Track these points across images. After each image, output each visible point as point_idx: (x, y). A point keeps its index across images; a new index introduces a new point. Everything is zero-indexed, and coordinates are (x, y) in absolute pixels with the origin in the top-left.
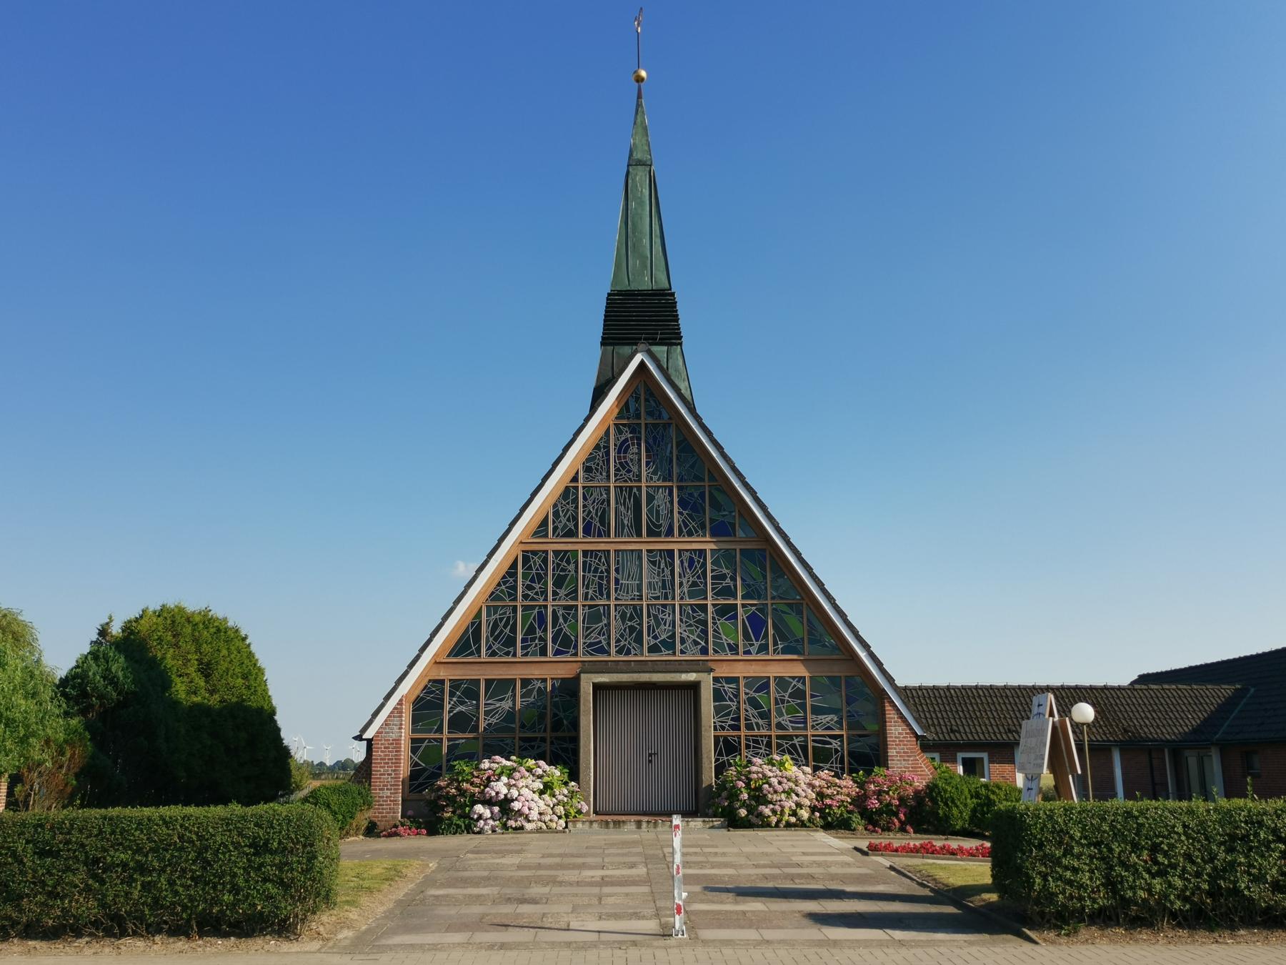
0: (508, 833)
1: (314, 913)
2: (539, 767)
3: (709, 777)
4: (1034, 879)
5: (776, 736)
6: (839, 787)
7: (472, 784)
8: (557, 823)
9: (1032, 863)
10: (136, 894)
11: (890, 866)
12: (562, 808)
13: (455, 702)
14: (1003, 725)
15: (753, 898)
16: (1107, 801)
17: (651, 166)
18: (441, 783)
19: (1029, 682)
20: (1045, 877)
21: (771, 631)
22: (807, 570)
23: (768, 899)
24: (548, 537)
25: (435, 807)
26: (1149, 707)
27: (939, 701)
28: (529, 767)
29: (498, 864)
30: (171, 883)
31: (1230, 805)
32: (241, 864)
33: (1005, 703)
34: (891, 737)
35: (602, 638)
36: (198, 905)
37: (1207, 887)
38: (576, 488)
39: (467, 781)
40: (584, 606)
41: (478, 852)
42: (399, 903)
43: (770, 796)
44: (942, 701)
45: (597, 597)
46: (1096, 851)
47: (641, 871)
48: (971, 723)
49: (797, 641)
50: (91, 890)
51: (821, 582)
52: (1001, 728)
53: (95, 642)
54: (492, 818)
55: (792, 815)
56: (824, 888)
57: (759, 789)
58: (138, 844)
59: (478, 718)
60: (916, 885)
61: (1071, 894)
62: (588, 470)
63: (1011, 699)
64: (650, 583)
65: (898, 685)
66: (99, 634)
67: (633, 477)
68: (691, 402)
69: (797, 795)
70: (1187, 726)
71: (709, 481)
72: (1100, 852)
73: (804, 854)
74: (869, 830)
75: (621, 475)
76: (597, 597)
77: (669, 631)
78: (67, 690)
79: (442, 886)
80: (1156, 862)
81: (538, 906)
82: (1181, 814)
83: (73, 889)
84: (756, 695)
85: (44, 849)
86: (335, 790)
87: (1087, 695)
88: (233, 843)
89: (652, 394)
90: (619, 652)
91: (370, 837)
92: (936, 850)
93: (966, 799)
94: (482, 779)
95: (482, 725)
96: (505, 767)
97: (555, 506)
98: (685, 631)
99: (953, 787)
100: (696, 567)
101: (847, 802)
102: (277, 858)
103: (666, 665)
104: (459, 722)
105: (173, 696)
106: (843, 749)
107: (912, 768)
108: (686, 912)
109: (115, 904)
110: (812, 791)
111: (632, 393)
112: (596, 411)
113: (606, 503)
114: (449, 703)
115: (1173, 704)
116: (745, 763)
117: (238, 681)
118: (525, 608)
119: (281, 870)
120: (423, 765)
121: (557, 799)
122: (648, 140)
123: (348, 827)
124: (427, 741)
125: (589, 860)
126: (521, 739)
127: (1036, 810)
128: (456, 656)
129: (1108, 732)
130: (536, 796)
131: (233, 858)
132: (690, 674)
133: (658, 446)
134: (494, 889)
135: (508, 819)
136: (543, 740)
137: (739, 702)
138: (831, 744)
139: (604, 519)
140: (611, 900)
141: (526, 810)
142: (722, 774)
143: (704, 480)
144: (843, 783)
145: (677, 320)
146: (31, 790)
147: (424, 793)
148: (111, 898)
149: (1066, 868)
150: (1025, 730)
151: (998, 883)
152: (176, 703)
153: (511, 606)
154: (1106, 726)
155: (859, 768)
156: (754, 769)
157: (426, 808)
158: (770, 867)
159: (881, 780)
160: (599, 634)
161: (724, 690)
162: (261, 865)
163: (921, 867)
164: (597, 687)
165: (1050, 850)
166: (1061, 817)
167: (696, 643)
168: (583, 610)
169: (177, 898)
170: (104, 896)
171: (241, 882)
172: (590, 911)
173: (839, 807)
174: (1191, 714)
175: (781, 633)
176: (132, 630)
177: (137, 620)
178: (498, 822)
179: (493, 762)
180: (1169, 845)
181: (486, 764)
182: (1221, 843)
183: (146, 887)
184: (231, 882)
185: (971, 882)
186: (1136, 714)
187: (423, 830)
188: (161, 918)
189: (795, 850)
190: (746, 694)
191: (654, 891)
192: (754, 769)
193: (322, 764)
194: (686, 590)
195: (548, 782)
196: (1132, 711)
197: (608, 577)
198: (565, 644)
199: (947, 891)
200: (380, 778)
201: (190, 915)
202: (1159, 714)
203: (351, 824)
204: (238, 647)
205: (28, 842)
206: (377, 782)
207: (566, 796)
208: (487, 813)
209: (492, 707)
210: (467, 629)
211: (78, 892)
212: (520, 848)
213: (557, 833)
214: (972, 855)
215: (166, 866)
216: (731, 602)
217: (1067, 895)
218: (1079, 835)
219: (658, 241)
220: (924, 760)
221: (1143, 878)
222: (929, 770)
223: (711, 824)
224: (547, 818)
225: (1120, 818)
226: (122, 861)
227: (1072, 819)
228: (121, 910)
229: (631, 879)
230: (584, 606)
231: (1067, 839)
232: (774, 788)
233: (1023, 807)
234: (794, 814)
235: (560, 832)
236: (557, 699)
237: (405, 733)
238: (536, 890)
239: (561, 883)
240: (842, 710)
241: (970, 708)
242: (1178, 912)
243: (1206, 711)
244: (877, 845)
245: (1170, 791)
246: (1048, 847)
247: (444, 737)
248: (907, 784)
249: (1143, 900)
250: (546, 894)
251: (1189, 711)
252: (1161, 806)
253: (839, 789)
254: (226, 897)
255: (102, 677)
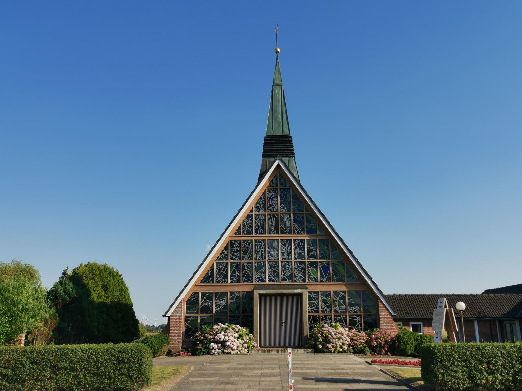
0: (224, 355)
1: (142, 388)
2: (237, 328)
3: (306, 332)
4: (438, 375)
5: (334, 315)
6: (360, 336)
7: (210, 335)
8: (244, 351)
9: (437, 369)
10: (70, 380)
11: (380, 369)
12: (246, 345)
13: (203, 301)
14: (428, 311)
15: (323, 383)
16: (469, 343)
17: (282, 86)
18: (198, 334)
19: (433, 293)
20: (443, 375)
21: (331, 272)
22: (346, 248)
23: (328, 383)
24: (241, 234)
25: (195, 344)
26: (489, 303)
27: (402, 301)
28: (233, 328)
29: (219, 368)
30: (84, 375)
31: (520, 344)
32: (112, 368)
33: (429, 302)
34: (381, 316)
35: (263, 275)
36: (95, 385)
37: (511, 379)
38: (252, 215)
39: (208, 334)
40: (255, 262)
41: (211, 363)
42: (178, 384)
43: (331, 340)
44: (403, 301)
45: (260, 258)
46: (465, 364)
47: (277, 371)
48: (415, 310)
49: (342, 276)
50: (52, 378)
51: (352, 252)
52: (428, 312)
53: (61, 277)
54: (218, 349)
55: (340, 348)
56: (352, 378)
57: (327, 337)
58: (71, 359)
59: (213, 308)
60: (391, 378)
61: (454, 382)
62: (257, 207)
63: (432, 300)
64: (282, 253)
65: (384, 294)
66: (63, 274)
67: (275, 210)
68: (298, 180)
69: (343, 340)
70: (505, 311)
71: (306, 211)
72: (466, 364)
73: (345, 364)
74: (372, 354)
75: (270, 209)
76: (260, 258)
77: (290, 272)
78: (50, 297)
79: (196, 377)
80: (490, 369)
81: (234, 385)
82: (500, 348)
83: (45, 378)
84: (326, 298)
85: (33, 361)
86: (155, 337)
87: (463, 299)
88: (109, 359)
89: (282, 177)
90: (270, 281)
91: (168, 356)
92: (400, 363)
93: (412, 341)
94: (214, 333)
95: (214, 311)
96: (223, 328)
97: (243, 222)
98: (296, 272)
99: (407, 337)
100: (301, 246)
101: (363, 342)
102: (127, 365)
103: (289, 286)
104: (205, 309)
105: (92, 299)
106: (361, 320)
107: (390, 328)
108: (294, 388)
109: (62, 384)
110: (349, 338)
111: (275, 176)
112: (260, 184)
113: (264, 220)
114: (201, 302)
115: (499, 302)
116: (321, 326)
117: (118, 293)
118: (232, 263)
119: (128, 370)
120: (191, 327)
121: (244, 341)
122: (280, 76)
123: (159, 352)
124: (192, 317)
125: (256, 366)
126: (230, 316)
127: (439, 346)
128: (204, 282)
129: (472, 314)
130: (236, 340)
131: (109, 365)
132: (298, 290)
133: (285, 197)
134: (217, 378)
135: (224, 349)
136: (239, 317)
137: (318, 301)
138: (357, 319)
139: (263, 227)
140: (264, 383)
141: (232, 346)
142: (312, 331)
143: (304, 211)
144: (361, 335)
145: (293, 147)
146: (35, 337)
147: (190, 338)
148: (60, 382)
149: (452, 371)
150: (435, 314)
151: (424, 377)
152: (93, 302)
153: (226, 262)
154: (471, 311)
155: (368, 328)
156: (325, 329)
157: (191, 344)
158: (331, 370)
159: (377, 333)
160: (261, 274)
161: (313, 296)
162: (120, 369)
163: (393, 370)
164: (261, 295)
165: (445, 363)
166: (450, 349)
167: (301, 277)
168: (255, 264)
169: (87, 381)
170: (58, 381)
171: (112, 375)
172: (255, 387)
173: (360, 345)
174: (507, 306)
175: (335, 273)
176: (76, 272)
177: (78, 268)
178: (220, 350)
179: (219, 326)
180: (495, 361)
181: (215, 326)
182: (517, 361)
183: (75, 377)
184: (108, 375)
185: (413, 376)
186: (484, 306)
187: (190, 354)
188: (80, 390)
189: (340, 362)
190: (321, 298)
191: (282, 379)
192: (325, 329)
193: (153, 326)
194: (296, 256)
195: (241, 334)
196: (482, 305)
197: (265, 250)
198: (248, 278)
199: (403, 380)
200: (173, 332)
201: (92, 389)
202: (493, 306)
203: (161, 351)
204: (118, 279)
205: (27, 358)
206: (172, 334)
207: (248, 340)
208: (216, 347)
209: (218, 303)
210: (208, 272)
211: (47, 379)
212: (228, 361)
213: (244, 355)
214: (415, 365)
215: (82, 368)
216: (315, 260)
217: (453, 382)
218: (457, 357)
219: (285, 116)
220: (395, 325)
221: (484, 375)
222: (397, 330)
223: (307, 351)
224: (240, 349)
225: (474, 350)
226: (65, 366)
227: (454, 350)
228: (64, 386)
229: (273, 374)
230: (255, 262)
231: (452, 358)
232: (333, 337)
233: (434, 345)
234: (341, 347)
235: (246, 354)
236: (245, 300)
237: (183, 314)
238: (234, 379)
239: (244, 376)
240: (361, 304)
241: (415, 304)
242: (500, 389)
243: (513, 305)
244: (375, 361)
245: (499, 338)
246: (444, 362)
247: (199, 316)
248: (388, 335)
249: (485, 384)
250: (238, 380)
251: (506, 305)
252: (492, 345)
253: (360, 337)
254: (106, 381)
255: (63, 291)
